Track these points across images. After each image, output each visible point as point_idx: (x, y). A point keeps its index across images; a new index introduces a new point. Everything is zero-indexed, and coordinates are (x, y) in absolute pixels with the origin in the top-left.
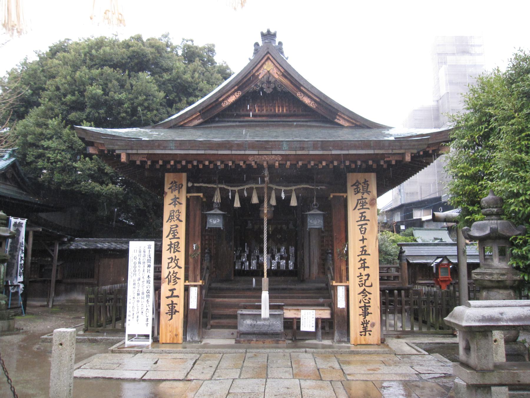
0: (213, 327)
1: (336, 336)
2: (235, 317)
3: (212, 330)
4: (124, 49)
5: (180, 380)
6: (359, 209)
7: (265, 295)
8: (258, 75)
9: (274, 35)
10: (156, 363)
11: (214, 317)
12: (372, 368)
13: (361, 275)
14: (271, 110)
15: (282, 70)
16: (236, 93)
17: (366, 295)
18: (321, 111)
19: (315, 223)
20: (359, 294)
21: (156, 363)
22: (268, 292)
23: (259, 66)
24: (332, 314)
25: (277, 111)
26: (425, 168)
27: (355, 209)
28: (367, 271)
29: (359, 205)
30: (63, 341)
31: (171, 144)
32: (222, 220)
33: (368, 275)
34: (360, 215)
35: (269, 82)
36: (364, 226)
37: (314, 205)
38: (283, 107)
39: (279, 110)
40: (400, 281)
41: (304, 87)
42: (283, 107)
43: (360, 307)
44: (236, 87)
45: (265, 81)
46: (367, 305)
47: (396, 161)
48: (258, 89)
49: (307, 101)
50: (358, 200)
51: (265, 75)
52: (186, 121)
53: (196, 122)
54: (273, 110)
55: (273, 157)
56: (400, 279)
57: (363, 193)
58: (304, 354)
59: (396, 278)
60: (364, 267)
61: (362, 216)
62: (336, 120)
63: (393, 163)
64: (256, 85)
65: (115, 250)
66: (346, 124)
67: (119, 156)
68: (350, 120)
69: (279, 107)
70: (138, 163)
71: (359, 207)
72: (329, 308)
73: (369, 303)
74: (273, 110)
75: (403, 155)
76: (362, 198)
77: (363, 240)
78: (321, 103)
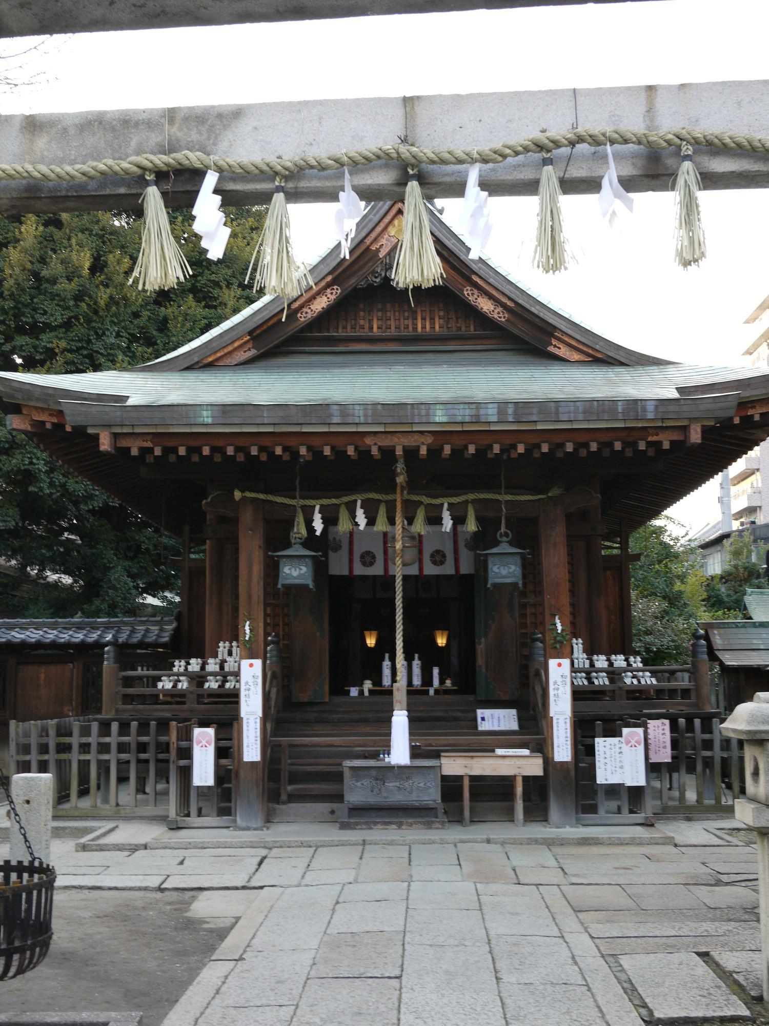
0: (292, 798)
1: (554, 813)
2: (338, 777)
3: (290, 805)
4: (39, 154)
5: (237, 888)
7: (400, 720)
8: (378, 250)
10: (182, 863)
11: (294, 778)
12: (623, 865)
14: (407, 327)
16: (329, 291)
18: (519, 329)
19: (504, 572)
21: (182, 863)
22: (406, 713)
23: (379, 229)
24: (546, 769)
26: (756, 448)
30: (32, 796)
31: (205, 413)
32: (311, 568)
37: (501, 536)
38: (432, 319)
40: (693, 700)
41: (480, 277)
42: (432, 319)
44: (329, 278)
47: (672, 443)
49: (485, 305)
52: (219, 355)
53: (242, 356)
54: (411, 328)
55: (416, 436)
56: (693, 695)
58: (485, 845)
59: (686, 693)
62: (551, 349)
63: (666, 445)
64: (374, 272)
65: (54, 645)
66: (576, 356)
67: (96, 437)
69: (424, 319)
70: (135, 452)
72: (539, 754)
74: (411, 328)
75: (685, 429)
78: (517, 310)
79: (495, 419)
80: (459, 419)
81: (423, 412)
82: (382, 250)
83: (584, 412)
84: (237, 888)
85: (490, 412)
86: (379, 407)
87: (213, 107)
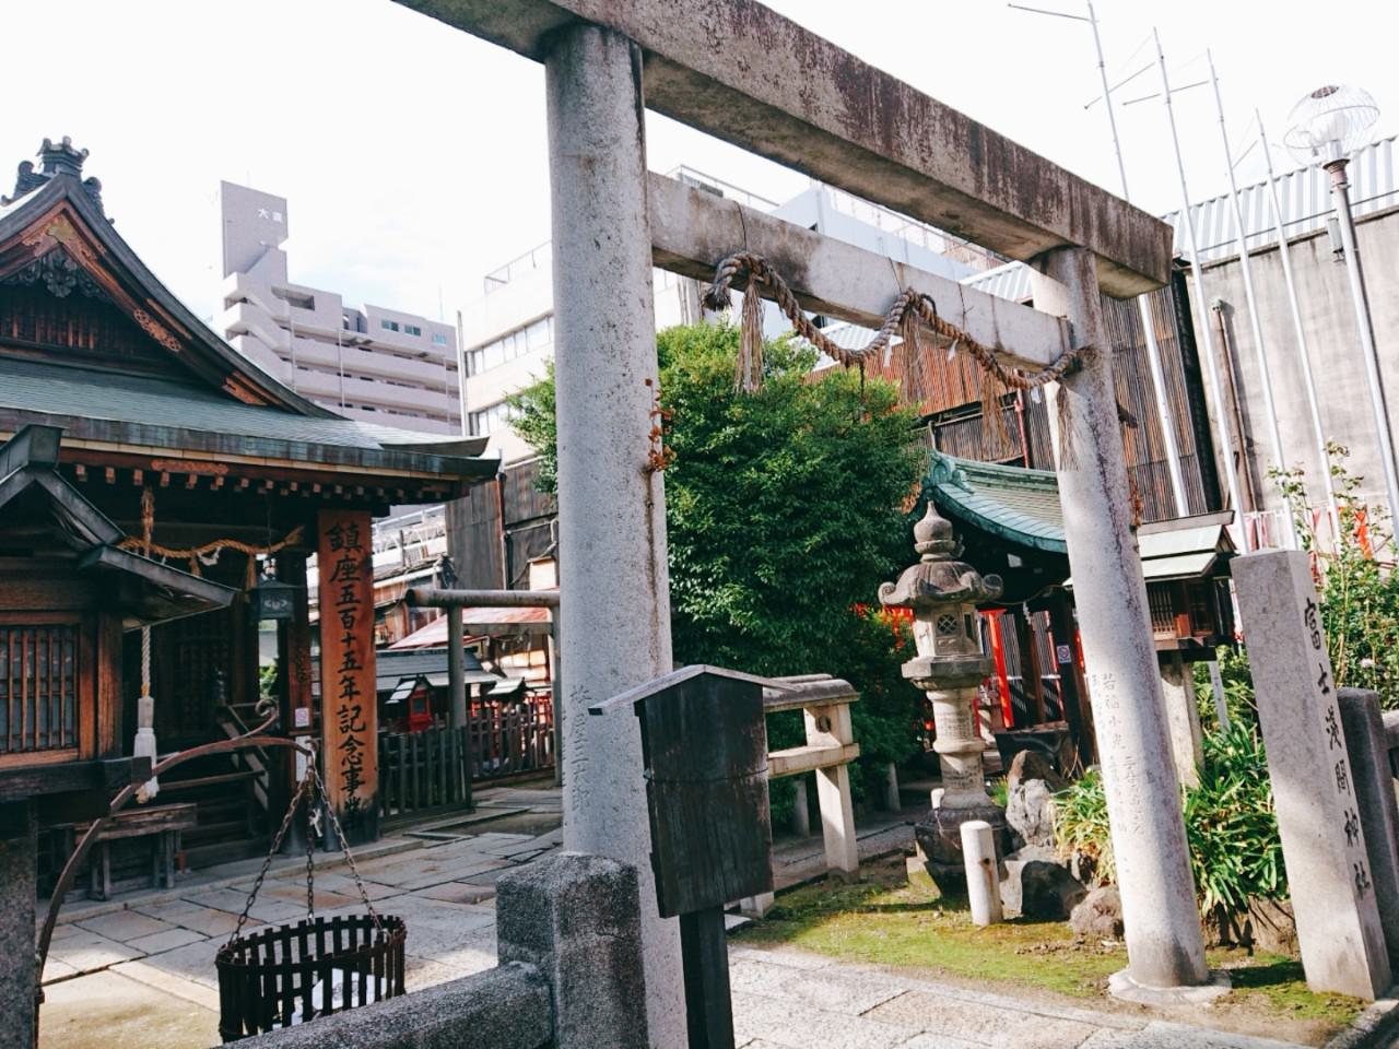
6: (341, 581)
8: (32, 248)
9: (78, 159)
13: (345, 710)
14: (55, 339)
15: (102, 250)
17: (354, 749)
20: (342, 747)
25: (71, 342)
27: (332, 580)
28: (357, 701)
29: (340, 573)
33: (358, 708)
34: (343, 592)
35: (60, 270)
36: (350, 614)
38: (86, 336)
39: (76, 342)
42: (86, 336)
43: (343, 774)
45: (51, 265)
46: (356, 767)
48: (31, 280)
49: (158, 332)
50: (339, 562)
51: (52, 250)
55: (210, 466)
57: (348, 549)
60: (350, 693)
61: (347, 594)
62: (226, 388)
64: (26, 271)
66: (250, 399)
68: (258, 390)
69: (76, 334)
71: (340, 576)
73: (359, 762)
76: (347, 559)
77: (348, 640)
78: (196, 343)
79: (305, 458)
80: (270, 454)
81: (233, 443)
82: (38, 248)
83: (384, 460)
84: (71, 977)
85: (301, 450)
86: (186, 433)
87: (551, 159)
